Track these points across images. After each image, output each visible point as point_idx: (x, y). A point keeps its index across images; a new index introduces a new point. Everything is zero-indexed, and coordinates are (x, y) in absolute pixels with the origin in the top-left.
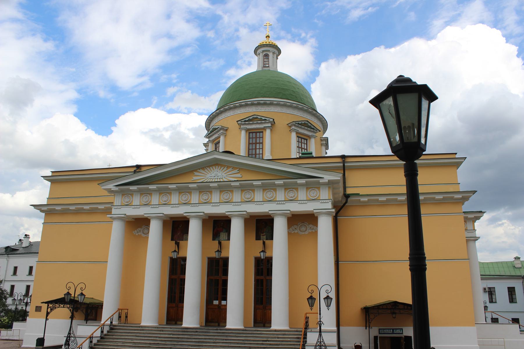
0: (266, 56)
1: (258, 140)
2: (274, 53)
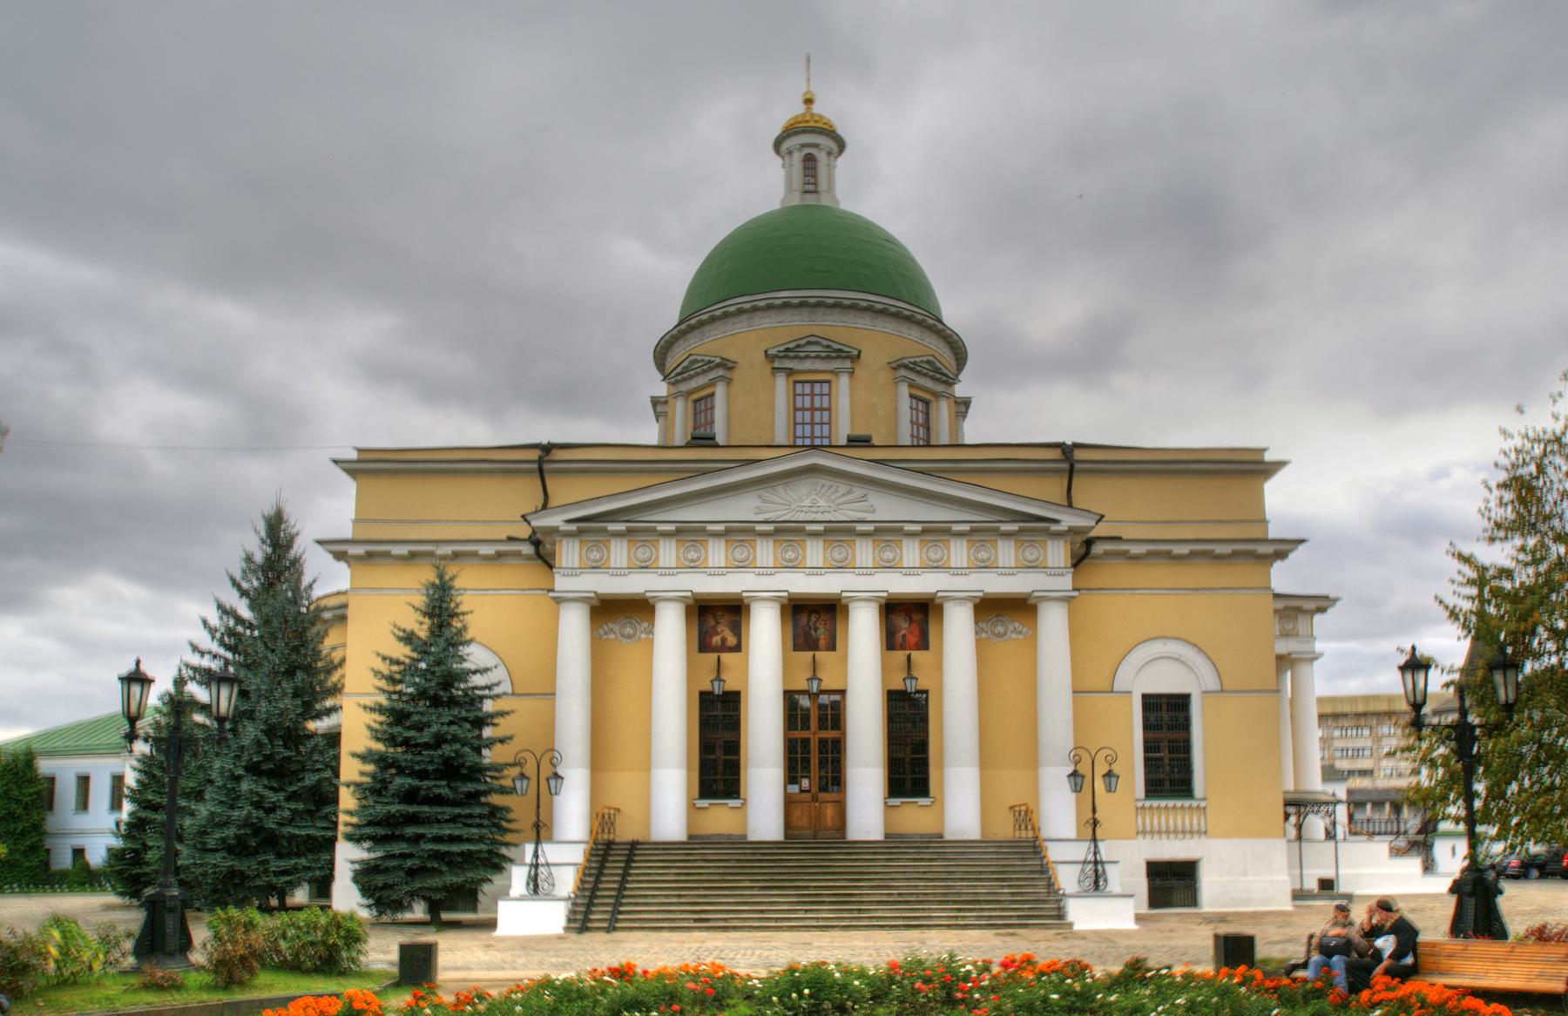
0: (810, 163)
1: (817, 399)
2: (829, 153)
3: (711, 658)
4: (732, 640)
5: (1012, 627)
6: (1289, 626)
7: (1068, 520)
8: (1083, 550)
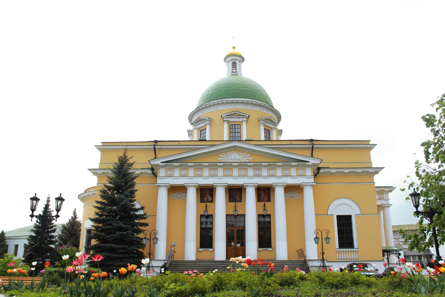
0: (234, 65)
1: (237, 129)
2: (240, 62)
3: (204, 204)
4: (210, 199)
5: (296, 195)
6: (381, 196)
7: (312, 161)
8: (317, 171)
